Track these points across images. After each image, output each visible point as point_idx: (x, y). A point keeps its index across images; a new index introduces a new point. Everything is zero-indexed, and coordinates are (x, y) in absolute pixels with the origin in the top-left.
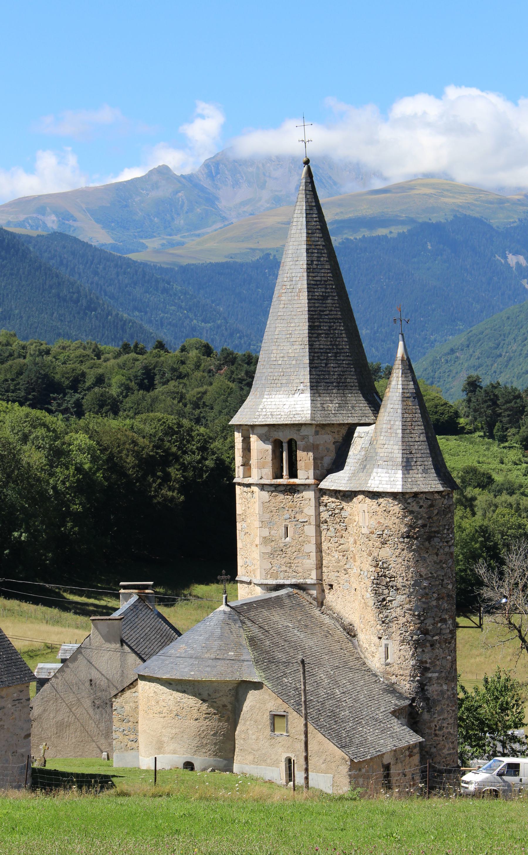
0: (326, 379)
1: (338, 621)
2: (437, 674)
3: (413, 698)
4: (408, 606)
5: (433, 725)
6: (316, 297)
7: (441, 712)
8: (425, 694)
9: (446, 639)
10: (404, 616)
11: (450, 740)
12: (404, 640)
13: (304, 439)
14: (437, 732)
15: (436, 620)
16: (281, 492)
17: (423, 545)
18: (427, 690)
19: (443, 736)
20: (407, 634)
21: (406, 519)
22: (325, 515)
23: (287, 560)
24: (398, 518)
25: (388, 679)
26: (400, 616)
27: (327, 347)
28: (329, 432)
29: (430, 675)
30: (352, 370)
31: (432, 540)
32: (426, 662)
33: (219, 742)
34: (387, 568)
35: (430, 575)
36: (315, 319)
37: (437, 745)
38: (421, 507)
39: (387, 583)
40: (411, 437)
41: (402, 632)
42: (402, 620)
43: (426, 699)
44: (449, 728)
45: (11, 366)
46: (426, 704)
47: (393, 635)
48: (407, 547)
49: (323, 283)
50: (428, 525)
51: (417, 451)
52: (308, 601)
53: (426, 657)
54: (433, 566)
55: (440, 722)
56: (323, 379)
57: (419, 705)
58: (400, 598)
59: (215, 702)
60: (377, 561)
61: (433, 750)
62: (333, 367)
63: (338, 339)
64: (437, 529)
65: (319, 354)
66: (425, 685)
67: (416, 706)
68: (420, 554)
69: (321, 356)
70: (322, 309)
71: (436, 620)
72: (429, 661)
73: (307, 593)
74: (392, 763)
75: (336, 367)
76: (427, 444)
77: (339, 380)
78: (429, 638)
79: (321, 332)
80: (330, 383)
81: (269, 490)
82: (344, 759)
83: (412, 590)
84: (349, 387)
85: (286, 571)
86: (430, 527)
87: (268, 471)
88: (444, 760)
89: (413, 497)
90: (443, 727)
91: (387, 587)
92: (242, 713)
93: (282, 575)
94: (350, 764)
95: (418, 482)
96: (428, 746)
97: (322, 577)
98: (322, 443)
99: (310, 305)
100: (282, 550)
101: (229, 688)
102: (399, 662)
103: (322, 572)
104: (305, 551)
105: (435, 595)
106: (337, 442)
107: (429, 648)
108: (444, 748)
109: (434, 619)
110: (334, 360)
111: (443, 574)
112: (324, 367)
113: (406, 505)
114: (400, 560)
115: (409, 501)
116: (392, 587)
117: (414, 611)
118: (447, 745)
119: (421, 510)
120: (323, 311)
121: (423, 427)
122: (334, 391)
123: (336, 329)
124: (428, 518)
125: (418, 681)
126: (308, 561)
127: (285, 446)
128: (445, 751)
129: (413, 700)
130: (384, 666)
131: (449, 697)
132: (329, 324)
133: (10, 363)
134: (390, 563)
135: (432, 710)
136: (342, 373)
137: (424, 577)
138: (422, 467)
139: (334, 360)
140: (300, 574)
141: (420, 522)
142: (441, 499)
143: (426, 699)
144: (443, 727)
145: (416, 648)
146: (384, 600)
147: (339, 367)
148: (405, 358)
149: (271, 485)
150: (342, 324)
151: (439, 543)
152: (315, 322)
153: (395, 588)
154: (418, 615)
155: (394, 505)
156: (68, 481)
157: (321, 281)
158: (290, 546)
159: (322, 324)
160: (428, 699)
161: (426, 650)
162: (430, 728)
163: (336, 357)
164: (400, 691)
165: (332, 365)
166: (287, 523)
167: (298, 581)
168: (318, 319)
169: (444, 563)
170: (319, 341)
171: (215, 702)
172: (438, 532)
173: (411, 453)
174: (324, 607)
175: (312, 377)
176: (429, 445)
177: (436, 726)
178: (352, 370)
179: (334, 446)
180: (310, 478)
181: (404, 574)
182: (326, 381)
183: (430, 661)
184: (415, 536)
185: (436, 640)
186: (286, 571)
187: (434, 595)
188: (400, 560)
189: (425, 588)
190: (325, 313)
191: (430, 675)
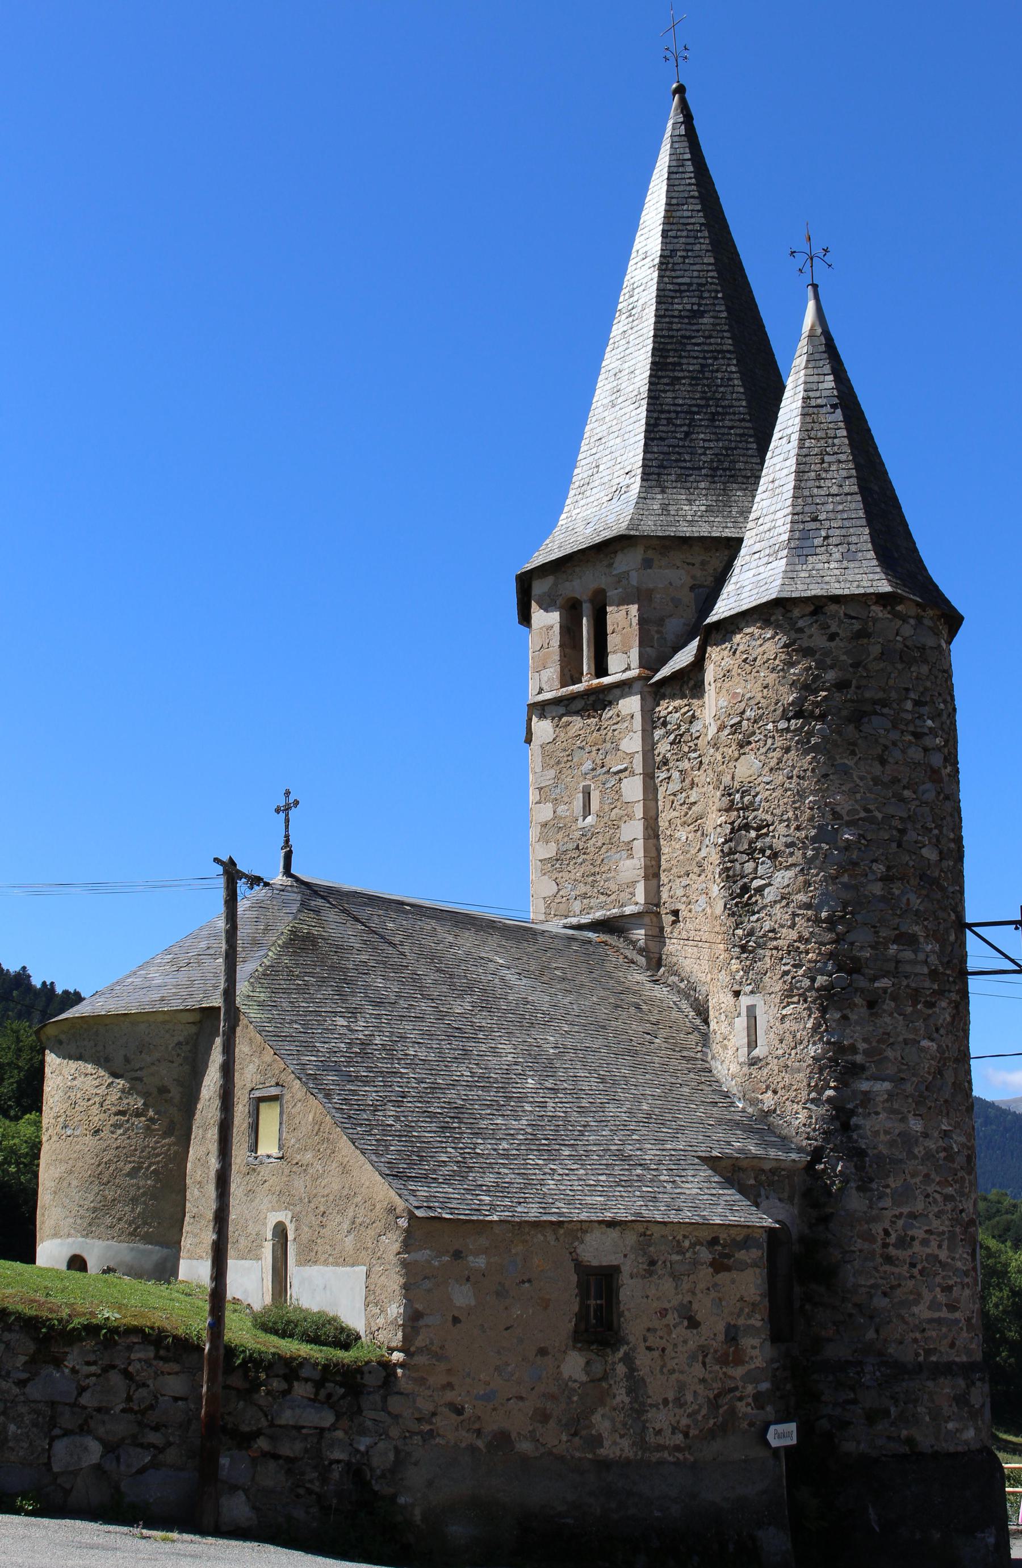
0: (685, 461)
1: (687, 997)
2: (887, 1085)
3: (816, 1147)
4: (802, 897)
5: (878, 1229)
6: (676, 313)
7: (904, 1195)
8: (850, 1138)
9: (916, 990)
10: (793, 926)
11: (938, 1279)
12: (791, 990)
13: (619, 581)
14: (892, 1251)
15: (882, 934)
16: (577, 713)
17: (839, 733)
18: (858, 1127)
19: (913, 1265)
20: (801, 972)
21: (792, 671)
22: (663, 748)
23: (587, 868)
24: (774, 669)
25: (754, 1102)
26: (782, 926)
27: (694, 402)
28: (679, 564)
29: (865, 1086)
30: (749, 446)
31: (866, 720)
32: (853, 1049)
33: (144, 1194)
34: (752, 803)
35: (863, 814)
36: (668, 351)
37: (892, 1288)
38: (832, 637)
39: (750, 843)
40: (818, 487)
41: (787, 968)
42: (790, 935)
43: (856, 1154)
44: (934, 1244)
45: (998, 1223)
46: (856, 1166)
47: (766, 979)
48: (797, 743)
49: (694, 287)
50: (854, 682)
51: (831, 515)
52: (626, 957)
53: (855, 1036)
54: (870, 791)
55: (900, 1223)
56: (676, 461)
57: (834, 1169)
58: (783, 878)
59: (140, 1079)
60: (730, 795)
61: (880, 1302)
62: (704, 440)
63: (722, 389)
64: (881, 695)
65: (673, 415)
66: (852, 1113)
67: (824, 1170)
68: (831, 758)
69: (676, 419)
70: (688, 334)
71: (882, 934)
72: (862, 1046)
73: (626, 939)
74: (626, 1270)
75: (710, 441)
76: (860, 499)
77: (715, 464)
78: (862, 982)
79: (680, 374)
80: (693, 469)
81: (554, 714)
82: (391, 1210)
83: (810, 853)
84: (740, 479)
85: (585, 896)
86: (858, 687)
87: (552, 673)
88: (918, 1335)
89: (814, 613)
90: (913, 1239)
91: (750, 852)
92: (199, 1106)
93: (577, 906)
94: (406, 1225)
95: (827, 579)
96: (863, 1290)
97: (660, 898)
98: (661, 586)
99: (660, 326)
100: (577, 848)
101: (176, 1040)
102: (780, 1052)
103: (659, 886)
104: (622, 839)
105: (880, 868)
106: (700, 586)
107: (864, 1011)
108: (916, 1302)
109: (876, 932)
110: (707, 427)
111: (905, 815)
112: (681, 439)
113: (794, 635)
114: (780, 778)
115: (801, 624)
116: (762, 851)
117: (818, 909)
118: (925, 1292)
119: (833, 644)
120: (690, 338)
121: (851, 465)
122: (702, 485)
123: (717, 371)
124: (851, 665)
125: (829, 1100)
126: (628, 862)
127: (587, 608)
128: (922, 1311)
129: (817, 1155)
130: (745, 1069)
131: (929, 1156)
132: (700, 361)
133: (997, 1219)
134: (757, 789)
135: (874, 1186)
136: (724, 452)
137: (846, 818)
138: (843, 548)
139: (707, 427)
140: (613, 897)
141: (830, 676)
142: (891, 621)
143: (856, 1154)
144: (913, 1239)
145: (823, 1010)
146: (745, 889)
147: (717, 441)
148: (819, 331)
149: (557, 701)
150: (735, 362)
151: (887, 730)
152: (668, 357)
153: (768, 852)
154: (829, 920)
155: (766, 640)
156: (1002, 1304)
157: (690, 284)
158: (593, 835)
159: (685, 361)
160: (861, 1153)
161: (854, 1017)
162: (869, 1237)
163: (713, 420)
164: (784, 1132)
165: (702, 436)
166: (588, 783)
167: (608, 913)
168: (675, 350)
169: (904, 788)
170: (673, 391)
171: (140, 1079)
172: (884, 703)
173: (815, 519)
174: (662, 969)
175: (649, 456)
176: (865, 501)
177: (887, 1233)
178: (749, 446)
179: (692, 595)
180: (632, 667)
181: (790, 814)
182: (683, 464)
183: (865, 1046)
184: (817, 711)
185: (885, 990)
186: (585, 896)
187: (875, 866)
188: (780, 778)
189: (848, 846)
190: (693, 341)
191: (865, 1086)
